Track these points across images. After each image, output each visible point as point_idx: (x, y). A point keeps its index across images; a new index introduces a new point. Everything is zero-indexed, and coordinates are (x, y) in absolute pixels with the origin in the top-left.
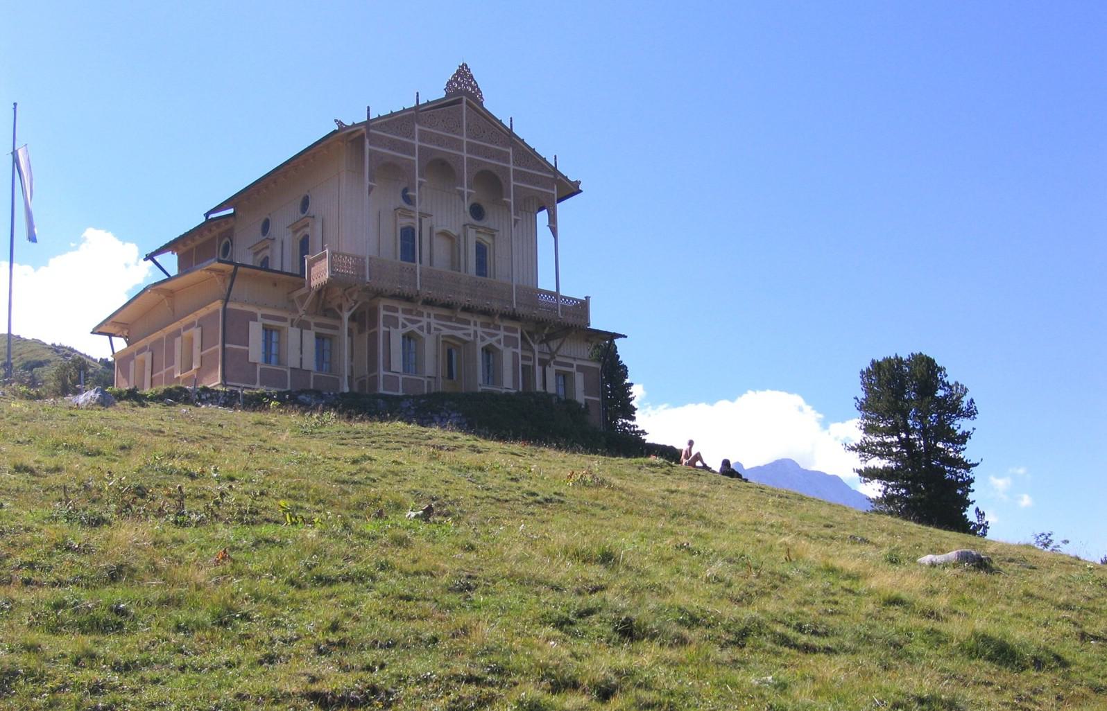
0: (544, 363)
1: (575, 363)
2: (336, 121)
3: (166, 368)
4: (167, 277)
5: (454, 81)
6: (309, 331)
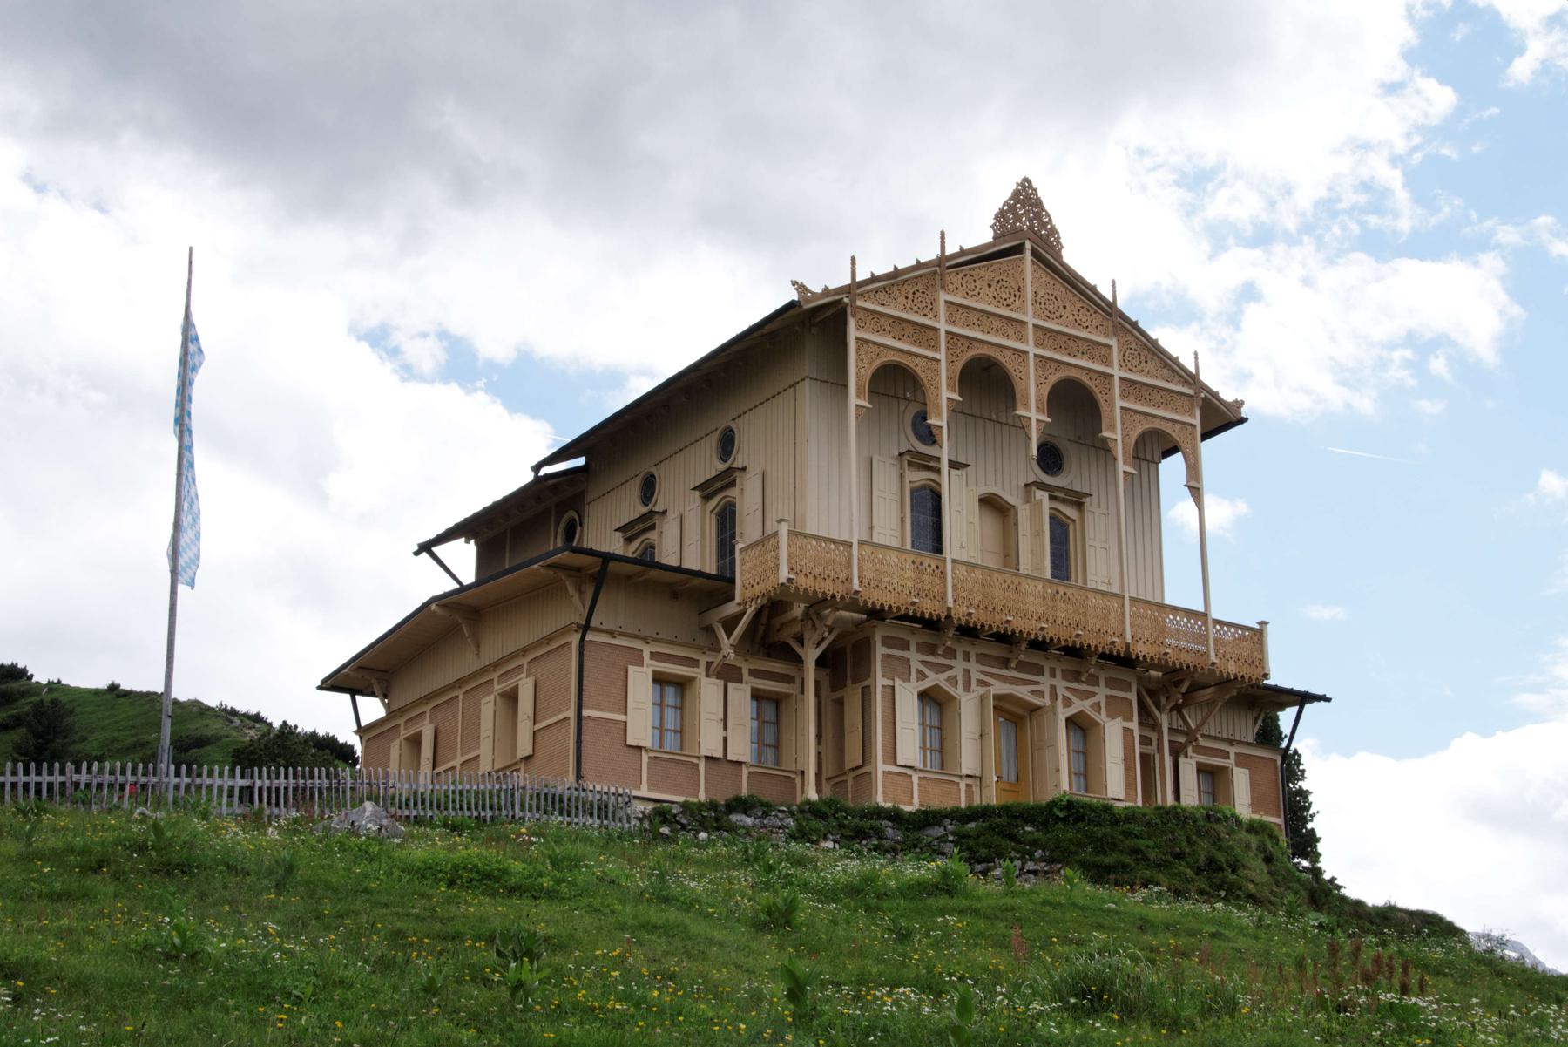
0: (1177, 751)
1: (1233, 751)
2: (794, 283)
3: (462, 755)
4: (457, 586)
5: (1008, 211)
6: (739, 685)
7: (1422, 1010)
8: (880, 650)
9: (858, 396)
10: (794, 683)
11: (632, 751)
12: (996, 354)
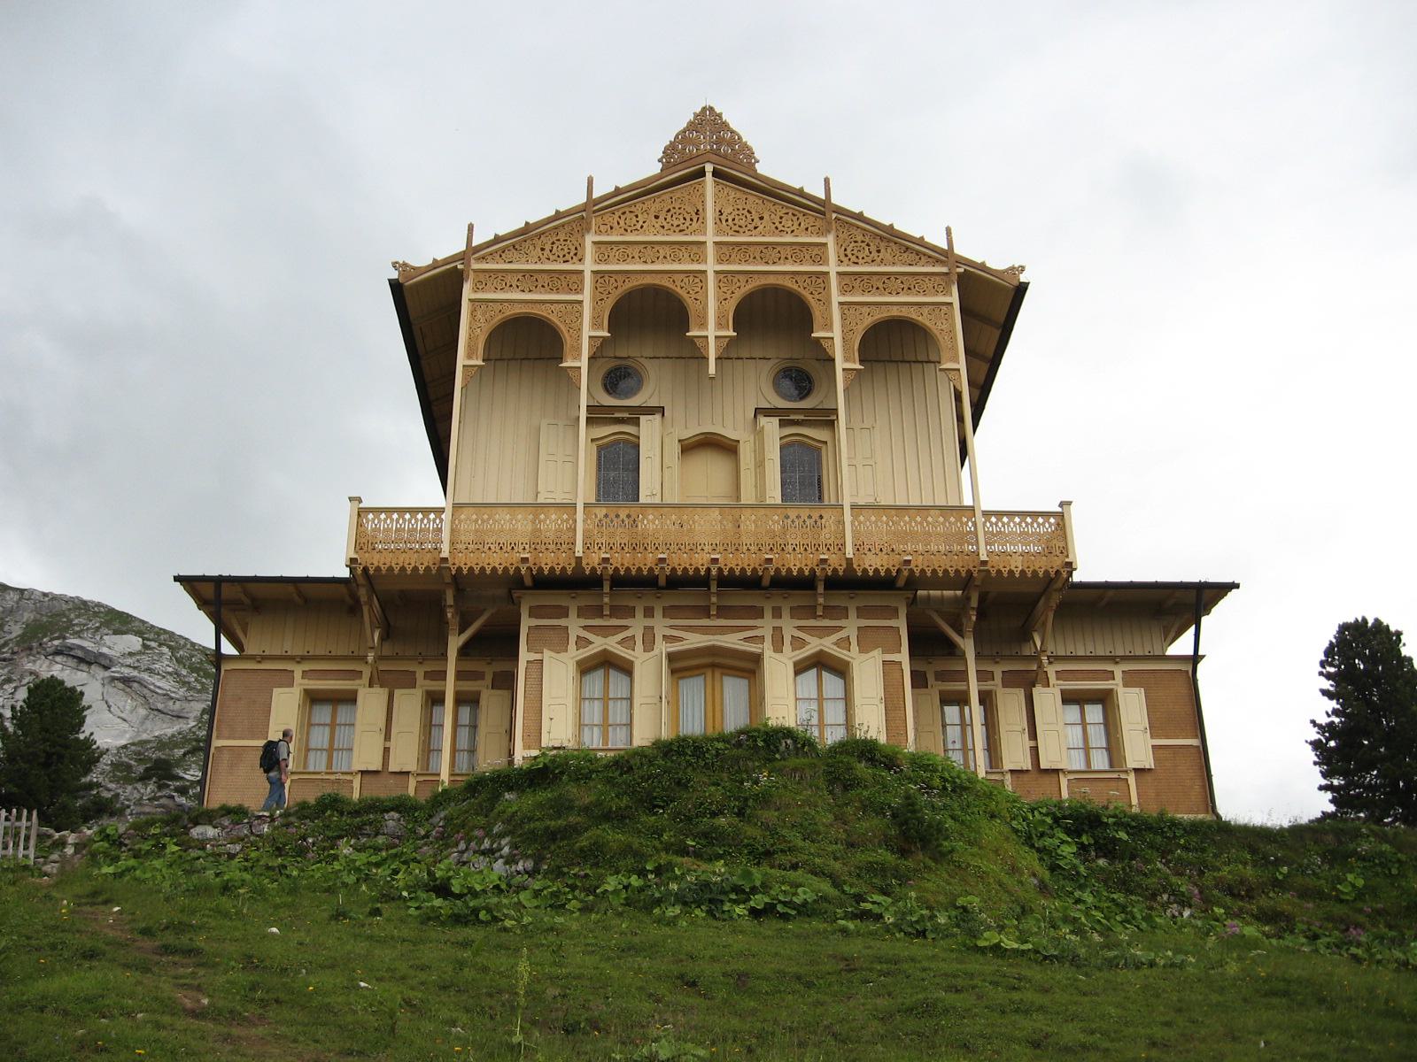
1: (1118, 670)
7: (287, 982)
8: (526, 623)
9: (846, 360)
10: (483, 679)
11: (393, 776)
12: (665, 282)
